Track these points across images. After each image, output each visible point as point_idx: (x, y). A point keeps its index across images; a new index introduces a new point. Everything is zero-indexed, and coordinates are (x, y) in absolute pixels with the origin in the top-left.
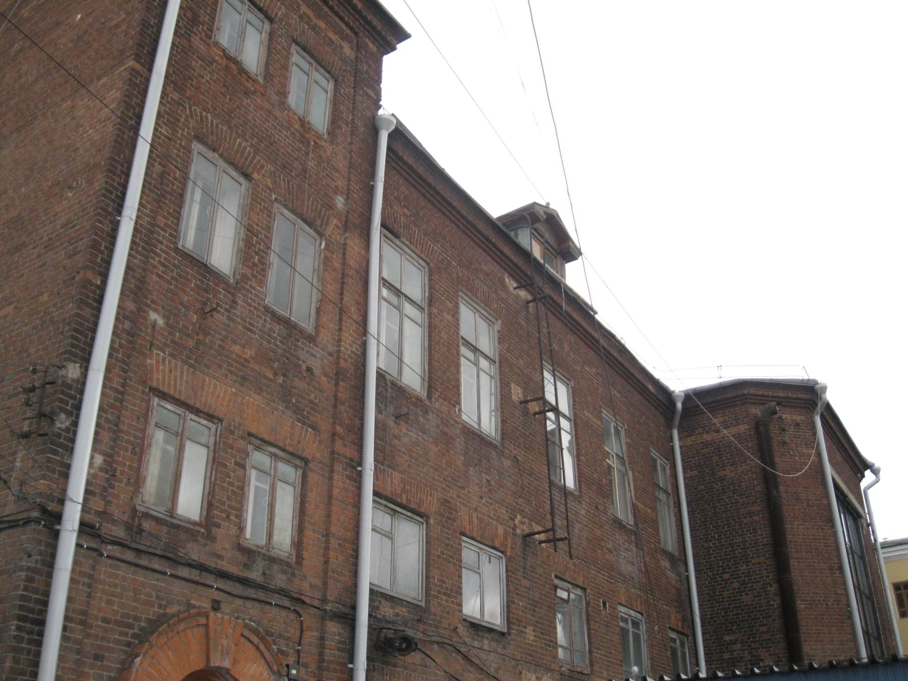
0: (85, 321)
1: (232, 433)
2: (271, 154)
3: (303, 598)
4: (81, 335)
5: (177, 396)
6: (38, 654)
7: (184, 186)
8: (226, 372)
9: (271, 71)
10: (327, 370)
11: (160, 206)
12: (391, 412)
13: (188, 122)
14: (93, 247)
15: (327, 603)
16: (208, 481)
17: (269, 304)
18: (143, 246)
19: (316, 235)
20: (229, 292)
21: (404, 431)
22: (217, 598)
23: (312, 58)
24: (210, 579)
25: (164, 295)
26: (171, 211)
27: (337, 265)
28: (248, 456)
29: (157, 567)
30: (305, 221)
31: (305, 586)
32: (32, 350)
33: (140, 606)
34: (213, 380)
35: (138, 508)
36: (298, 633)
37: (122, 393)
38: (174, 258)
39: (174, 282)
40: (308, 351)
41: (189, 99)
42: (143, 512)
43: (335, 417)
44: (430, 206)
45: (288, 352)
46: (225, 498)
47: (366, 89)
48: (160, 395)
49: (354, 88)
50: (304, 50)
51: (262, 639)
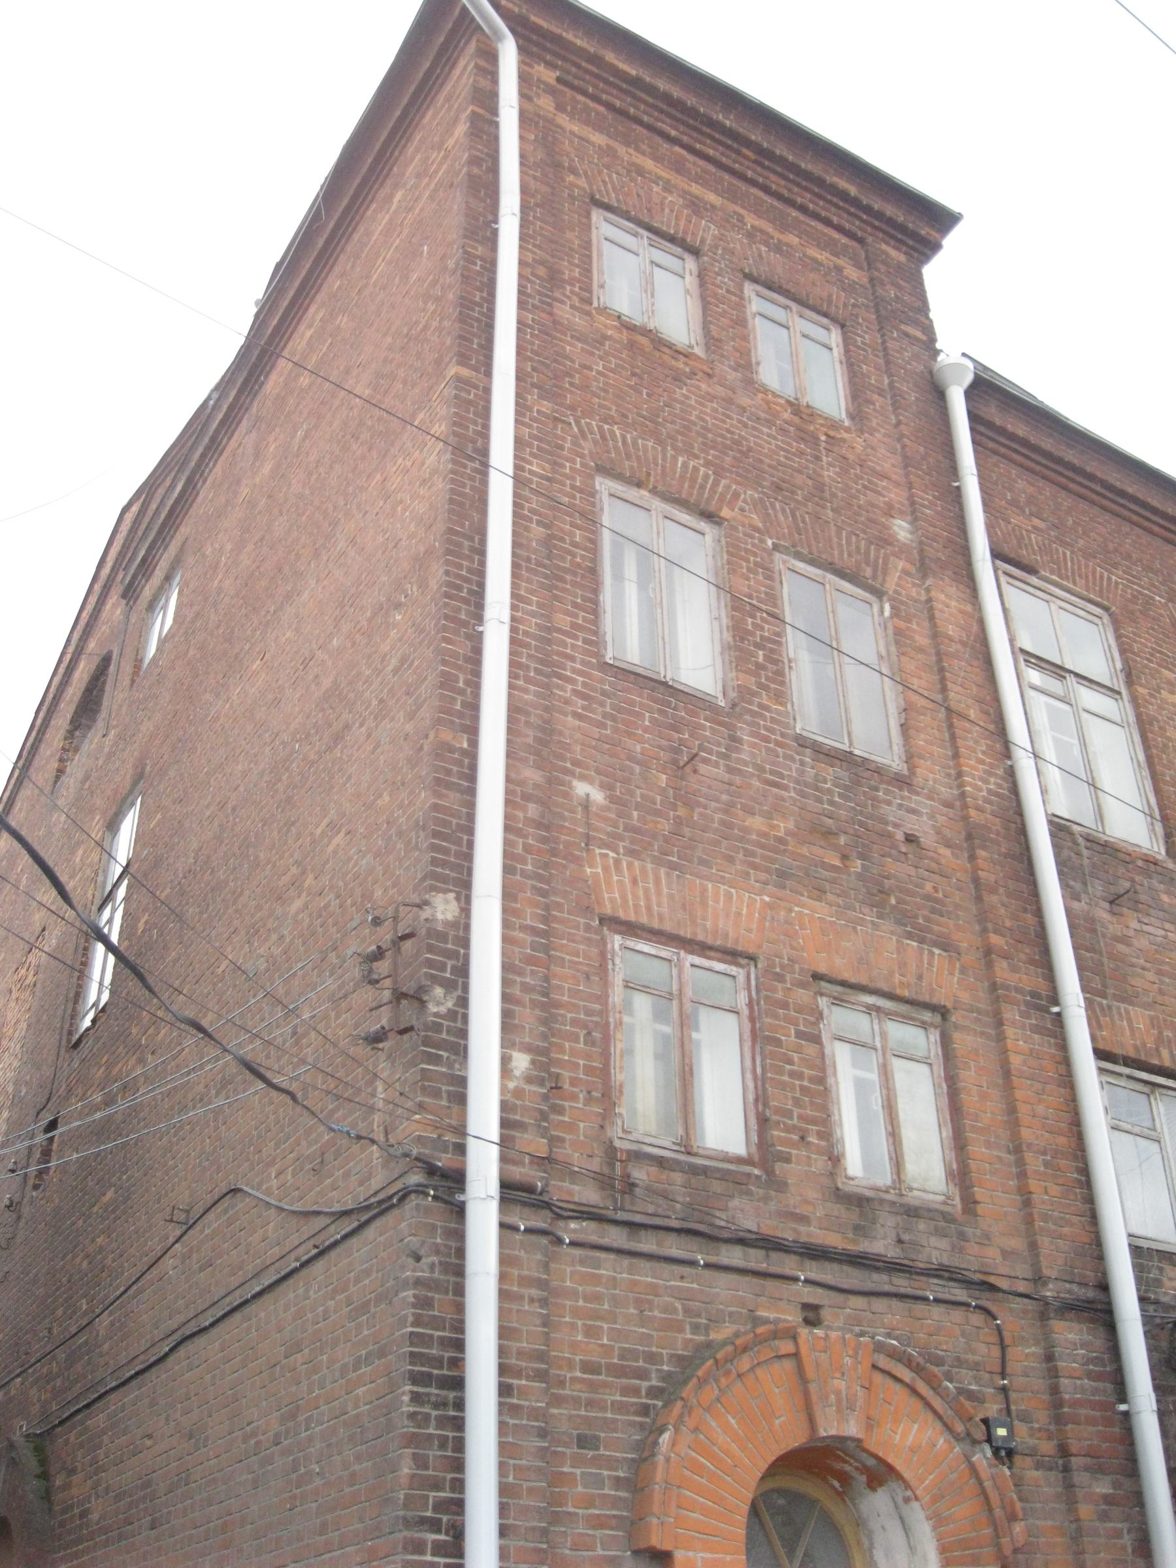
0: (452, 816)
1: (780, 978)
2: (747, 471)
3: (992, 1279)
4: (449, 842)
5: (656, 925)
6: (460, 1445)
7: (595, 554)
8: (745, 868)
9: (714, 333)
10: (948, 833)
11: (555, 595)
12: (1099, 894)
13: (580, 446)
14: (442, 686)
15: (1045, 1284)
16: (749, 1076)
17: (805, 734)
18: (536, 669)
19: (867, 595)
20: (720, 724)
21: (1134, 924)
22: (811, 1300)
23: (787, 297)
24: (788, 1265)
25: (594, 748)
26: (579, 600)
27: (922, 640)
28: (822, 1019)
29: (675, 1252)
30: (841, 574)
31: (992, 1255)
32: (378, 893)
33: (654, 1333)
34: (723, 887)
35: (618, 1144)
36: (996, 1352)
37: (545, 934)
38: (602, 681)
39: (609, 723)
40: (900, 806)
41: (572, 408)
42: (629, 1152)
43: (983, 917)
44: (1084, 505)
45: (861, 813)
46: (790, 1102)
47: (903, 327)
48: (623, 928)
49: (879, 330)
50: (770, 288)
51: (918, 1370)
